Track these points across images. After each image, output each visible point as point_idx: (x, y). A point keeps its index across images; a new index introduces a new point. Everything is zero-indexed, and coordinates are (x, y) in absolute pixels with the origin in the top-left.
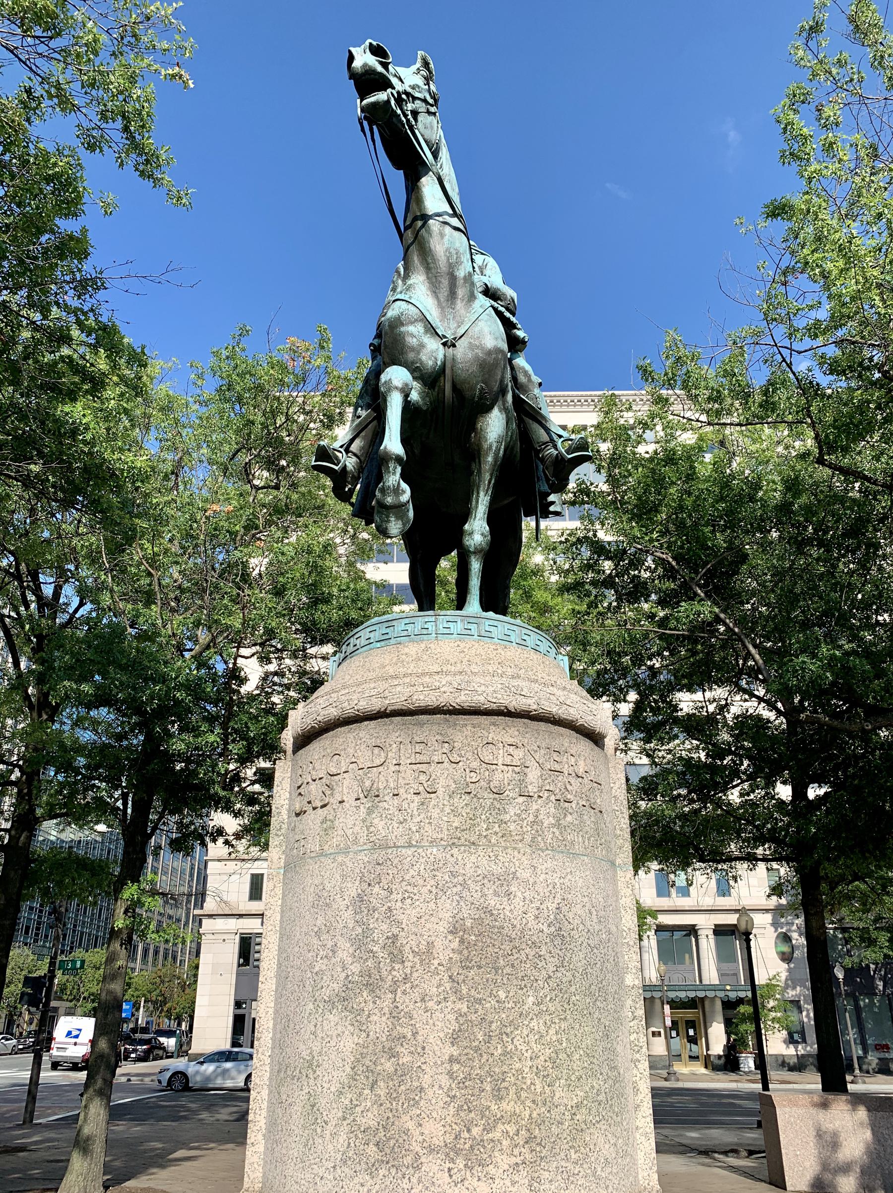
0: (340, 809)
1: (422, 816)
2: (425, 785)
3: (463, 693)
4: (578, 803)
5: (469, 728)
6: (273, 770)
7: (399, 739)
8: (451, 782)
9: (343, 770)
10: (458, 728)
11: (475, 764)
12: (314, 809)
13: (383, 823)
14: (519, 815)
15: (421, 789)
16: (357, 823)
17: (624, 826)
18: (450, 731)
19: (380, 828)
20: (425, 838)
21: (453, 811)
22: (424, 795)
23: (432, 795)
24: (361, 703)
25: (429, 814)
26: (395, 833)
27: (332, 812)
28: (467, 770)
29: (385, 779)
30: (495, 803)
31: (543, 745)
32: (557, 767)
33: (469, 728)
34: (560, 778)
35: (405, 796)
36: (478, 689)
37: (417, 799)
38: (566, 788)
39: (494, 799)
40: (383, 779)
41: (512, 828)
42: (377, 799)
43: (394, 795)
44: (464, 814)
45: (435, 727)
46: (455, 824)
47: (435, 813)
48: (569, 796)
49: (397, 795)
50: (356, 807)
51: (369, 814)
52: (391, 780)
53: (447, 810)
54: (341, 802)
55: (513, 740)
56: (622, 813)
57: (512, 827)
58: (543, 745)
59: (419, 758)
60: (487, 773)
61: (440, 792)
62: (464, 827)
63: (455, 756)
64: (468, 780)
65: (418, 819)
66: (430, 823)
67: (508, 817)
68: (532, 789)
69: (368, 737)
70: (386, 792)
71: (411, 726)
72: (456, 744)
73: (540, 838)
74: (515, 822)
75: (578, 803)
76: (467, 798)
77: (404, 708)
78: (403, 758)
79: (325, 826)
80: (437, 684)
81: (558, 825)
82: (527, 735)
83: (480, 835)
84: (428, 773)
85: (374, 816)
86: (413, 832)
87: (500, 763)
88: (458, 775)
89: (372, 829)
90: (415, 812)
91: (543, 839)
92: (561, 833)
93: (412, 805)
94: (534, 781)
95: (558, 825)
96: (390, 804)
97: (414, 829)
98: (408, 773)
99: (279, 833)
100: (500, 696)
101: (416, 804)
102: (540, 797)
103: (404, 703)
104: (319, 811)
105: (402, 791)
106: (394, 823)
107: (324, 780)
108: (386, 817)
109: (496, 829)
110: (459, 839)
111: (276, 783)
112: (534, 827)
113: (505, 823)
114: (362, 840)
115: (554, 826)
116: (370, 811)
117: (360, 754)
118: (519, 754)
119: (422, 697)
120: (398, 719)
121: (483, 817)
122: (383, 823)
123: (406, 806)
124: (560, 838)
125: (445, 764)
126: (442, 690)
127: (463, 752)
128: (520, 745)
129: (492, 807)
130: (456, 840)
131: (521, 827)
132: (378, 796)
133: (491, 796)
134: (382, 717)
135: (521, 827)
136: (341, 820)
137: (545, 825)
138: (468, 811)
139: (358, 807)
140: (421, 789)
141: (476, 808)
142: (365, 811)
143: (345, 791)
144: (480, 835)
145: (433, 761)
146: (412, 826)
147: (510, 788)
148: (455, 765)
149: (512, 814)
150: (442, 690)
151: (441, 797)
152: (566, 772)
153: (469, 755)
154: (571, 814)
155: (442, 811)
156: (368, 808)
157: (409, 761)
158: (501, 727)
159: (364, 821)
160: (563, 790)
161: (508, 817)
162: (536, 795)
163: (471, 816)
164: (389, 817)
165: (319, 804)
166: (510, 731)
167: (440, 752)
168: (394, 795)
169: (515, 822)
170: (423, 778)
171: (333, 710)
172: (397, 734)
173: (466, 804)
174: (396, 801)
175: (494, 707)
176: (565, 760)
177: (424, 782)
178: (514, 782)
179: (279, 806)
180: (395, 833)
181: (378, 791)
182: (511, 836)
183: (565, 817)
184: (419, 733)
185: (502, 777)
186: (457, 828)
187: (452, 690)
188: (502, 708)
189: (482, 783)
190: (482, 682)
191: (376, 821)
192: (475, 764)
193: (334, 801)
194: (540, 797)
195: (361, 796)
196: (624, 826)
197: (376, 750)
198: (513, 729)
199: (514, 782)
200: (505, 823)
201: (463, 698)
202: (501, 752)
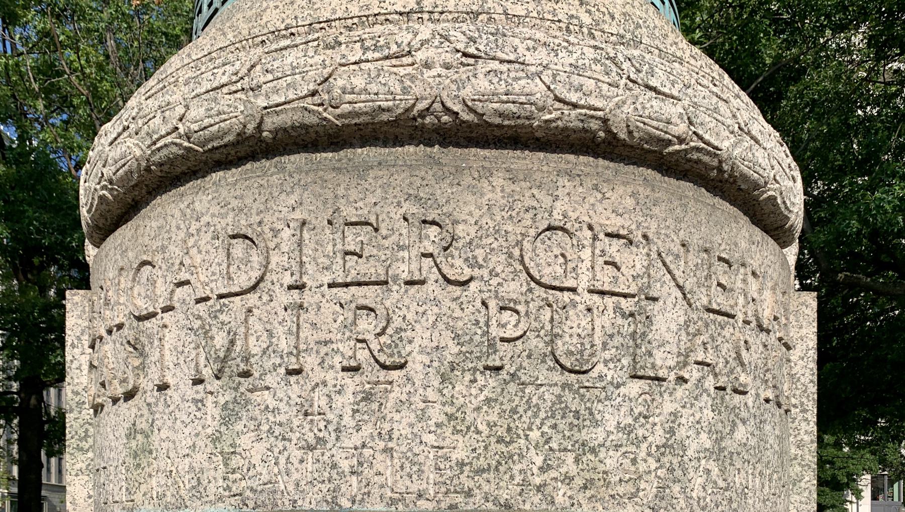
0: (161, 407)
1: (367, 430)
2: (375, 346)
3: (482, 67)
4: (758, 395)
5: (498, 180)
6: (116, 326)
7: (298, 215)
8: (447, 339)
9: (161, 303)
10: (467, 180)
11: (514, 288)
12: (115, 401)
13: (261, 447)
14: (628, 430)
15: (363, 355)
16: (200, 443)
17: (807, 438)
18: (443, 191)
19: (256, 460)
20: (376, 491)
21: (450, 417)
22: (372, 372)
23: (395, 374)
24: (192, 114)
25: (387, 426)
26: (296, 476)
27: (145, 411)
28: (492, 304)
29: (265, 328)
30: (568, 396)
31: (695, 241)
32: (720, 301)
33: (498, 180)
34: (727, 333)
35: (318, 375)
36: (529, 59)
37: (351, 383)
38: (739, 357)
39: (565, 386)
40: (259, 327)
41: (610, 463)
42: (246, 383)
43: (290, 372)
44: (482, 427)
45: (401, 178)
46: (459, 454)
47: (402, 423)
48: (743, 378)
49: (298, 372)
50: (195, 401)
51: (226, 421)
52: (280, 330)
53: (436, 414)
54: (163, 387)
55: (619, 221)
56: (804, 411)
57: (611, 460)
58: (695, 241)
59: (358, 268)
60: (547, 314)
61: (417, 364)
62: (482, 463)
63: (458, 262)
64: (495, 331)
65: (356, 440)
66: (387, 451)
67: (599, 435)
68: (663, 361)
69: (215, 209)
70: (268, 365)
71: (330, 176)
72: (460, 230)
73: (676, 488)
74: (617, 447)
75: (758, 395)
76: (492, 382)
77: (312, 120)
78: (310, 268)
79: (133, 444)
80: (405, 38)
81: (717, 453)
82: (656, 210)
83: (525, 483)
84: (381, 311)
85: (239, 427)
86: (342, 474)
87: (583, 284)
88: (465, 317)
89: (235, 462)
90: (348, 420)
91: (684, 490)
92: (722, 471)
93: (339, 401)
94: (668, 337)
95: (717, 453)
96: (278, 396)
97: (345, 465)
98: (327, 311)
99: (83, 444)
100: (590, 84)
101: (348, 398)
102: (682, 380)
103: (308, 103)
104: (123, 406)
105: (310, 362)
106: (291, 447)
107: (125, 331)
108: (270, 431)
109: (569, 465)
110: (469, 494)
111: (69, 340)
112: (665, 460)
113: (593, 451)
114: (212, 489)
115: (709, 453)
116: (229, 415)
117: (198, 259)
118: (633, 261)
119: (359, 82)
120: (298, 159)
121: (535, 435)
122: (261, 447)
123: (323, 402)
124: (721, 484)
125: (430, 287)
126: (420, 56)
127: (480, 253)
128: (638, 237)
129: (559, 408)
130: (460, 499)
131: (634, 461)
132: (246, 374)
133: (558, 377)
134: (253, 157)
135: (634, 461)
136: (163, 435)
137: (690, 453)
138: (493, 417)
139: (199, 403)
140: (363, 355)
141: (514, 411)
142: (217, 412)
143: (169, 359)
144: (525, 483)
145: (396, 278)
146: (339, 456)
147: (607, 355)
148: (457, 291)
149: (611, 425)
150: (420, 56)
151: (418, 379)
152: (740, 317)
153: (498, 261)
154: (744, 422)
155: (422, 416)
156: (225, 407)
157: (327, 279)
158: (589, 183)
159: (215, 439)
160: (733, 364)
161: (599, 435)
162: (672, 377)
163: (501, 432)
164: (278, 430)
165: (120, 391)
166: (613, 196)
167: (414, 252)
168: (290, 372)
169: (617, 447)
170: (367, 325)
171: (130, 142)
172: (291, 201)
173: (488, 401)
174: (295, 389)
175: (571, 118)
176: (739, 284)
177: (370, 337)
178: (618, 340)
179: (79, 389)
180: (296, 476)
181: (246, 360)
182: (608, 485)
183: (732, 431)
184: (354, 194)
185: (588, 324)
186: (461, 464)
187: (449, 58)
188: (594, 125)
189: (535, 343)
190: (540, 35)
191: (245, 441)
192: (514, 288)
193: (147, 384)
194: (682, 380)
195: (207, 373)
196: (807, 438)
197: (239, 247)
198: (620, 190)
199: (618, 340)
200: (593, 451)
201: (483, 84)
202: (586, 254)
